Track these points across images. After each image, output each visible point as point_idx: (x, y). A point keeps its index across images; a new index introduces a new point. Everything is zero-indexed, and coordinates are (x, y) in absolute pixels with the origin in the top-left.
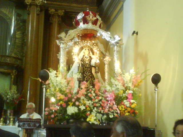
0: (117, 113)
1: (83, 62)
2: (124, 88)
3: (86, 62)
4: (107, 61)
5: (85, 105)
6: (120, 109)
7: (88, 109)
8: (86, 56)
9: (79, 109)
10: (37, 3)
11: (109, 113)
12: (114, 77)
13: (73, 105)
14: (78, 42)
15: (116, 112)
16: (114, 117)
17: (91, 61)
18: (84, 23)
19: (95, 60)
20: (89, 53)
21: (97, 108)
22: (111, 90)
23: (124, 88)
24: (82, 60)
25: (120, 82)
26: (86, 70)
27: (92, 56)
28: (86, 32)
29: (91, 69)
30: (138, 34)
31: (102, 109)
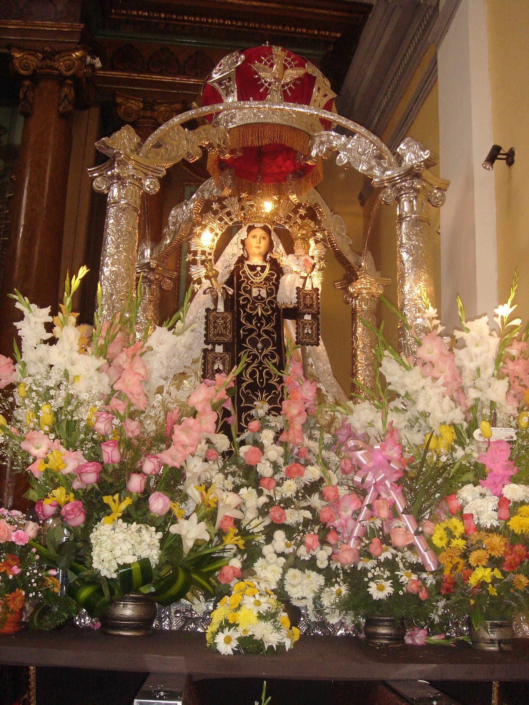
0: (418, 568)
1: (239, 289)
2: (458, 416)
3: (255, 292)
4: (363, 299)
5: (210, 516)
6: (437, 542)
7: (231, 542)
8: (256, 261)
9: (171, 545)
10: (62, 68)
11: (365, 571)
12: (399, 349)
13: (127, 517)
14: (220, 200)
15: (414, 559)
16: (396, 593)
17: (277, 286)
18: (242, 97)
19: (302, 273)
20: (271, 246)
21: (289, 537)
22: (379, 425)
23: (458, 416)
24: (235, 279)
25: (435, 379)
26: (251, 331)
27: (287, 261)
28: (252, 141)
29: (279, 328)
30: (516, 158)
31: (324, 542)
